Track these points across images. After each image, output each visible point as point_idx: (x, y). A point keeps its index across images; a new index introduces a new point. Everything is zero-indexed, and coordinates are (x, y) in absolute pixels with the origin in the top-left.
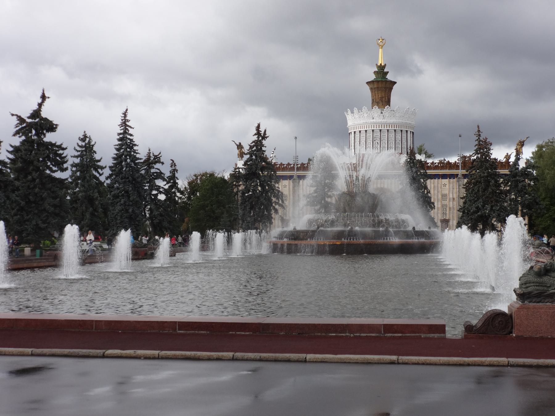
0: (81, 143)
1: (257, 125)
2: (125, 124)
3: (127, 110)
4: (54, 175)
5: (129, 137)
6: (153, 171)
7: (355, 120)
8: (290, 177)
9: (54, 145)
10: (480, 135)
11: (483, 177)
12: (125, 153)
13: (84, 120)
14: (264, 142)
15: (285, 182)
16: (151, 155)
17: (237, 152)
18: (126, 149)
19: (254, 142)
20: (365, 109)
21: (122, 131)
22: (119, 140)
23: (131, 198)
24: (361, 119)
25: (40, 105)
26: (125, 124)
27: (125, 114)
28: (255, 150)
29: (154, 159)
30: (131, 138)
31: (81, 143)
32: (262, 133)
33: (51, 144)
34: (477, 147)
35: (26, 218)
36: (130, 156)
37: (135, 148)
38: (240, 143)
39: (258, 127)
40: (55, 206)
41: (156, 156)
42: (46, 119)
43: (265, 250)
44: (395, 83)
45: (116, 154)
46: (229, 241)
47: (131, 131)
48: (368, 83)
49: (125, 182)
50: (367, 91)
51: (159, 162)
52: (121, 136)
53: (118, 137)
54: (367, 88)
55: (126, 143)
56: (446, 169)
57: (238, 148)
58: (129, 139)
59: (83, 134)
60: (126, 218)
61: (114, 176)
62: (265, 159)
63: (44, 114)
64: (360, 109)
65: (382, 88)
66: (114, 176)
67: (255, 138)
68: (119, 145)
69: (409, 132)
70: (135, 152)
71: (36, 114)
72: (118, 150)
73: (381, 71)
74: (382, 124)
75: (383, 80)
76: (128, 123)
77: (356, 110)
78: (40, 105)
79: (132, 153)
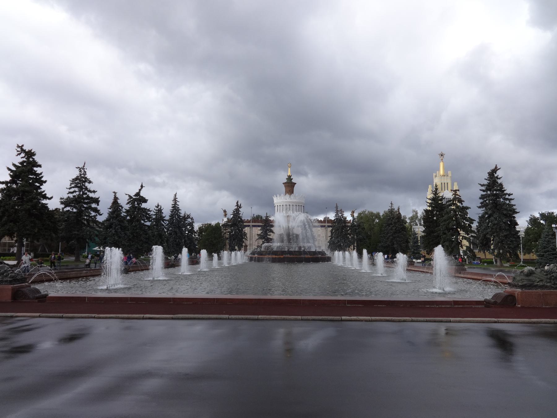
0: (156, 209)
2: (175, 200)
4: (145, 223)
6: (186, 222)
7: (278, 200)
8: (249, 226)
9: (146, 209)
13: (158, 198)
15: (246, 228)
17: (224, 214)
20: (282, 195)
23: (177, 234)
24: (279, 200)
25: (140, 190)
26: (175, 200)
27: (175, 195)
31: (156, 209)
33: (144, 208)
35: (132, 244)
36: (178, 215)
39: (237, 202)
40: (146, 239)
42: (142, 197)
43: (245, 260)
46: (236, 255)
47: (178, 203)
50: (283, 189)
51: (189, 218)
54: (283, 185)
55: (175, 209)
62: (240, 217)
63: (141, 194)
64: (280, 195)
65: (290, 186)
67: (236, 207)
71: (138, 194)
73: (290, 178)
74: (290, 202)
77: (278, 195)
78: (140, 190)
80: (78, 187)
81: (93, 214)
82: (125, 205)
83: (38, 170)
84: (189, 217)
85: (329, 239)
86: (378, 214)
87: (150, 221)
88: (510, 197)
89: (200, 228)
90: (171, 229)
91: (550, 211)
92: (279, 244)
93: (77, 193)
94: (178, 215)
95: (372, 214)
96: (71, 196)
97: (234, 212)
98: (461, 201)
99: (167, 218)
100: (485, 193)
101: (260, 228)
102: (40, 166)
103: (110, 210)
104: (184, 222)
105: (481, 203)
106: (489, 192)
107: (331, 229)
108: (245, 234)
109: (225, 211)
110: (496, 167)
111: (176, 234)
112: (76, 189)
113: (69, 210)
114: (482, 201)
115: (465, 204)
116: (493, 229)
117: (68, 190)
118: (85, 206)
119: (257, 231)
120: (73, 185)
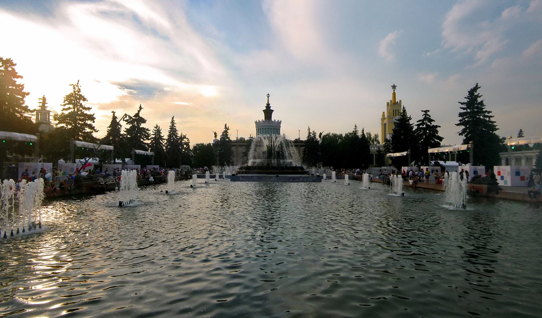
4: (144, 141)
47: (175, 125)
62: (228, 138)
71: (137, 115)
73: (268, 106)
78: (139, 111)
80: (72, 104)
81: (88, 130)
82: (124, 127)
83: (18, 81)
84: (185, 137)
85: (302, 155)
86: (341, 135)
87: (149, 139)
88: (490, 115)
89: (194, 147)
93: (72, 110)
95: (335, 136)
96: (66, 112)
98: (431, 121)
99: (166, 137)
100: (465, 111)
101: (243, 147)
102: (21, 77)
103: (109, 129)
104: (181, 142)
105: (460, 121)
106: (469, 110)
107: (304, 148)
108: (233, 152)
109: (215, 133)
110: (477, 86)
112: (71, 106)
113: (63, 127)
114: (461, 118)
115: (433, 123)
117: (63, 107)
118: (80, 122)
120: (66, 102)
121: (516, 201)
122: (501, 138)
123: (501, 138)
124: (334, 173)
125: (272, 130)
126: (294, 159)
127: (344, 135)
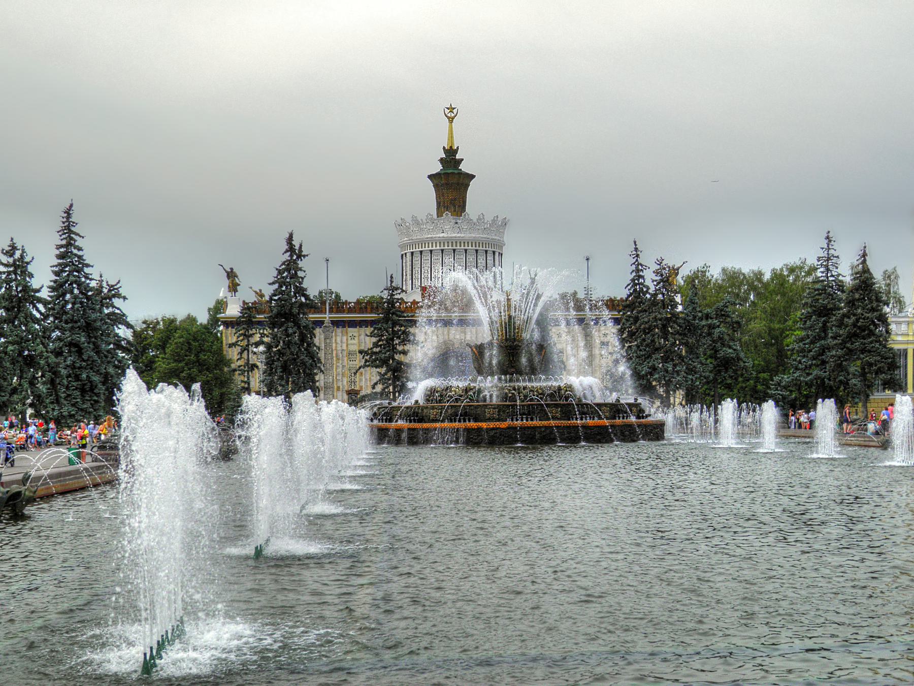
1: (288, 236)
3: (71, 206)
5: (75, 251)
10: (637, 256)
11: (660, 320)
12: (72, 278)
14: (301, 264)
16: (104, 284)
17: (227, 282)
18: (71, 272)
19: (283, 264)
21: (64, 242)
22: (61, 256)
27: (68, 213)
28: (287, 276)
29: (110, 291)
30: (80, 253)
32: (297, 247)
34: (634, 274)
36: (79, 285)
37: (86, 270)
38: (232, 269)
41: (112, 286)
44: (473, 177)
45: (55, 281)
47: (79, 242)
48: (430, 177)
49: (72, 328)
51: (118, 295)
52: (62, 250)
53: (57, 252)
56: (367, 312)
57: (228, 277)
58: (76, 255)
59: (9, 243)
60: (76, 389)
61: (51, 319)
66: (51, 319)
67: (287, 256)
68: (60, 264)
69: (497, 254)
70: (87, 278)
72: (57, 274)
73: (451, 158)
75: (456, 172)
76: (73, 229)
79: (83, 279)
90: (57, 333)
91: (737, 267)
92: (430, 383)
94: (79, 285)
97: (280, 272)
101: (369, 330)
111: (80, 352)
116: (55, 304)
119: (362, 339)
121: (76, 490)
122: (203, 318)
123: (203, 318)
124: (239, 417)
125: (490, 258)
126: (591, 368)
127: (767, 276)
